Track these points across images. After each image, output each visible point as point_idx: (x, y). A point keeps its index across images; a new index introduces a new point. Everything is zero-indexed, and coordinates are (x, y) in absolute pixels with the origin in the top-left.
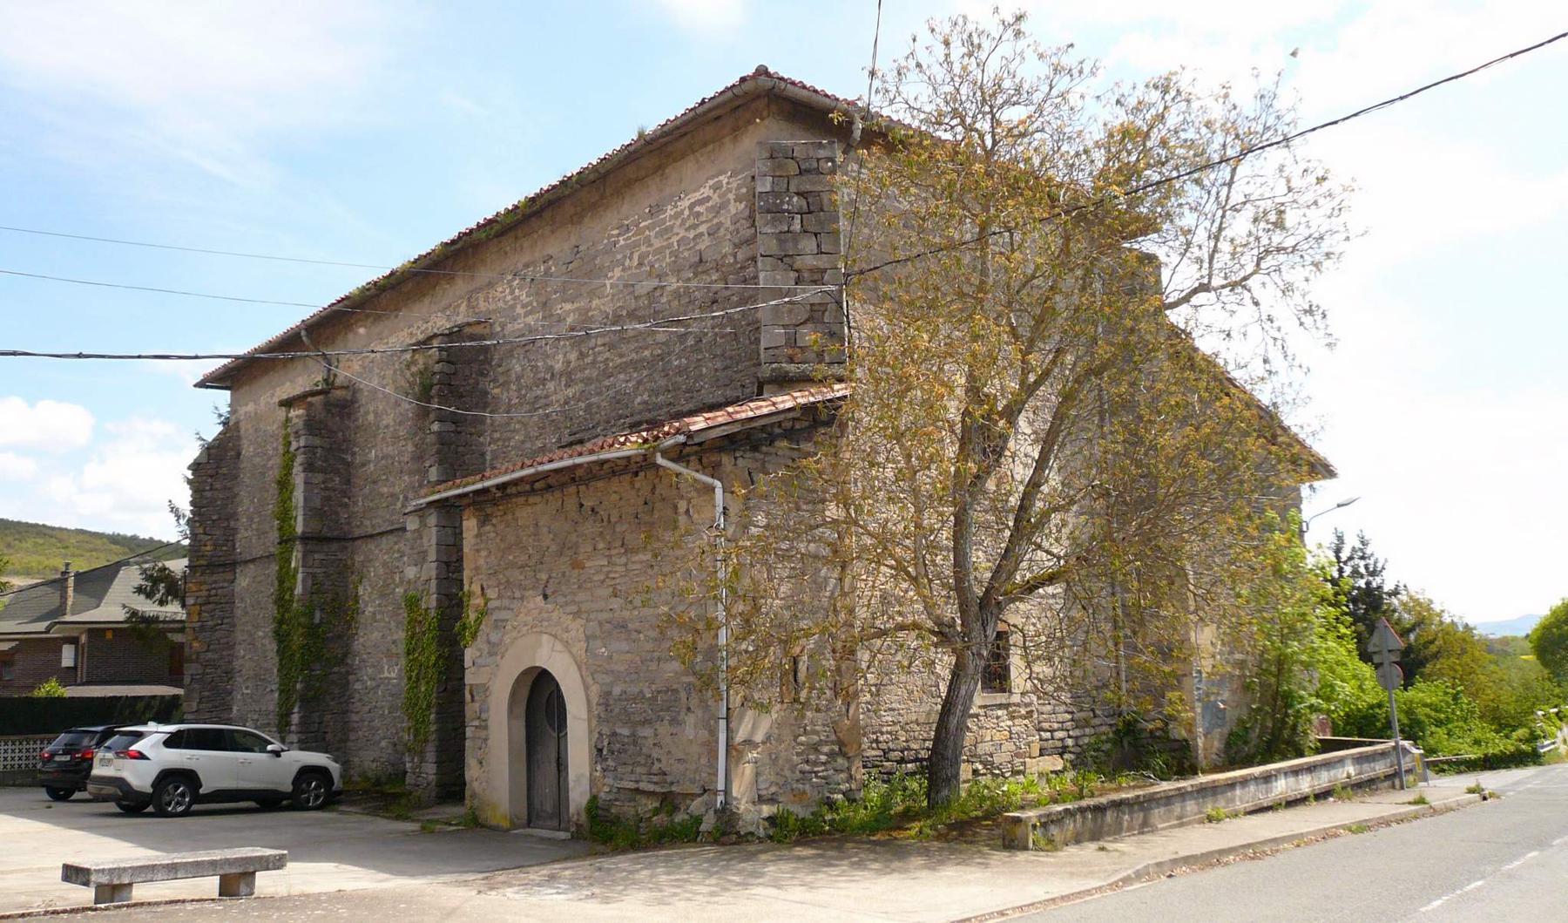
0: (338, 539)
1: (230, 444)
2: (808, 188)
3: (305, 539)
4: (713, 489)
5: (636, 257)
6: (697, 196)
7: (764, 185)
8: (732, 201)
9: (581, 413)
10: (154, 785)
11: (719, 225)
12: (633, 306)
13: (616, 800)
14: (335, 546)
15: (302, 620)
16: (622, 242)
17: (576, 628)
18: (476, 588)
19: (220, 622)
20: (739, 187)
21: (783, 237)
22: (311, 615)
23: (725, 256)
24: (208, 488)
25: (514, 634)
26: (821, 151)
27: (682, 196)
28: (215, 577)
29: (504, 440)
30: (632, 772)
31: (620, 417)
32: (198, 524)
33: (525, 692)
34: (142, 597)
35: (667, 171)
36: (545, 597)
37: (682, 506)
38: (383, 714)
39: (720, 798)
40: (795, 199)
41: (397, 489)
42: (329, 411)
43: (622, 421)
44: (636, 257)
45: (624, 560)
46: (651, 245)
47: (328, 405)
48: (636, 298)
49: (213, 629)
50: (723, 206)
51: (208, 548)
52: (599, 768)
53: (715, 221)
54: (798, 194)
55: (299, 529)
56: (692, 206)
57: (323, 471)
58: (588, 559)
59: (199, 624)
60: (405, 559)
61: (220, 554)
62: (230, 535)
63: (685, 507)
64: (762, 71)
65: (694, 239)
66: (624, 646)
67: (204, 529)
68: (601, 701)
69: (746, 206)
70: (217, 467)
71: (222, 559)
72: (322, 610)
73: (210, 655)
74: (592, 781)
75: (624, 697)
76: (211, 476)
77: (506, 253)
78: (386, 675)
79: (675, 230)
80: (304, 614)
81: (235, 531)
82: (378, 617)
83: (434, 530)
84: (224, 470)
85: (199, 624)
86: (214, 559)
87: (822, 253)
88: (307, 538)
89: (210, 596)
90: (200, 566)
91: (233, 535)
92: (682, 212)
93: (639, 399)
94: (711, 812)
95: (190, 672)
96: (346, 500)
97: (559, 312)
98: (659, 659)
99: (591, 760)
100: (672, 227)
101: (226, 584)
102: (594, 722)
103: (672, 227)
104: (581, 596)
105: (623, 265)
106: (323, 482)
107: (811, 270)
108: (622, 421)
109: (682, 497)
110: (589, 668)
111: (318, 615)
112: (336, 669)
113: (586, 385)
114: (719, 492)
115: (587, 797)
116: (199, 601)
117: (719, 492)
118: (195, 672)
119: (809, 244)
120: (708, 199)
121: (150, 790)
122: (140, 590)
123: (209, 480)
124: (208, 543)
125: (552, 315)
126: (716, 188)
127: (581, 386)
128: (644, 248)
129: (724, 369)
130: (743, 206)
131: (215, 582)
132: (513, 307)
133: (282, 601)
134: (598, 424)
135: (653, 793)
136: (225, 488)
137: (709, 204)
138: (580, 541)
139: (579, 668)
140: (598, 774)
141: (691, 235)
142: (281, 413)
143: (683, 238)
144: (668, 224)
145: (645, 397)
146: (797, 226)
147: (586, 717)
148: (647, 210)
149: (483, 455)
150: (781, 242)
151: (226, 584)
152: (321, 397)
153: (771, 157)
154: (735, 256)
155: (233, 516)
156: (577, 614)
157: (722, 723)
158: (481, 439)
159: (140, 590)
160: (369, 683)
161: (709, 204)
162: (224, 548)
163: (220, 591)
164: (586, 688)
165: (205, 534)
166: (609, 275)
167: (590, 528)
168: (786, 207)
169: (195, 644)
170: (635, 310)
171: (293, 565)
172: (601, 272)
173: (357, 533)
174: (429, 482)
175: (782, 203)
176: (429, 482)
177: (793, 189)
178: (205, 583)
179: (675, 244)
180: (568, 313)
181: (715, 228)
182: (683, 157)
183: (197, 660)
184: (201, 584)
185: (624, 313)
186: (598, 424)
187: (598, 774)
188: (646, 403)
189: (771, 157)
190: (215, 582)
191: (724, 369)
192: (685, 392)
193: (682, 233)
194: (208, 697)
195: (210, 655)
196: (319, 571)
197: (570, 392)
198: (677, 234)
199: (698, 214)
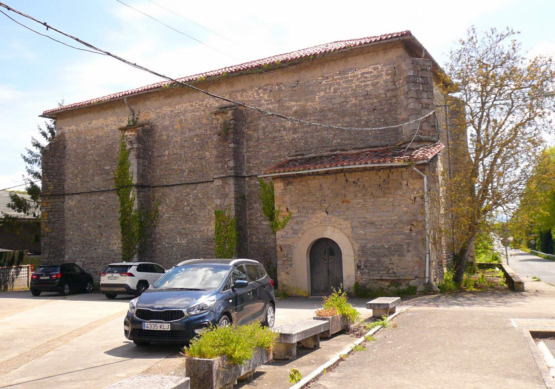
0: (148, 186)
1: (61, 143)
2: (424, 75)
3: (137, 186)
4: (422, 178)
5: (332, 89)
6: (365, 70)
7: (411, 73)
8: (384, 75)
9: (302, 144)
10: (137, 287)
11: (378, 83)
12: (332, 107)
13: (369, 283)
14: (147, 189)
15: (138, 219)
16: (324, 83)
17: (346, 224)
18: (283, 209)
19: (58, 219)
20: (387, 70)
21: (418, 91)
22: (140, 217)
23: (381, 94)
24: (51, 161)
25: (309, 226)
26: (427, 63)
27: (357, 69)
28: (54, 200)
29: (255, 152)
30: (378, 273)
31: (325, 147)
32: (46, 177)
33: (310, 248)
34: (10, 209)
35: (348, 59)
36: (327, 213)
37: (405, 183)
38: (177, 258)
39: (427, 280)
40: (420, 79)
41: (184, 168)
42: (143, 134)
43: (326, 149)
44: (332, 89)
45: (373, 200)
46: (341, 86)
47: (144, 131)
48: (333, 104)
49: (54, 222)
50: (379, 76)
51: (51, 188)
52: (359, 272)
53: (375, 81)
54: (421, 77)
55: (135, 181)
56: (362, 74)
57: (143, 158)
58: (352, 200)
59: (48, 220)
60: (191, 196)
61: (57, 190)
62: (61, 183)
63: (406, 183)
64: (408, 33)
65: (364, 86)
66: (374, 230)
67: (49, 179)
68: (360, 249)
69: (391, 77)
70: (55, 152)
71: (58, 192)
72: (144, 215)
73: (53, 234)
74: (356, 277)
75: (373, 247)
76: (52, 156)
77: (254, 79)
78: (179, 242)
79: (354, 82)
80: (138, 217)
81: (64, 181)
82: (172, 219)
83: (232, 186)
84: (58, 154)
85: (48, 220)
86: (54, 192)
87: (428, 98)
88: (139, 186)
89: (52, 208)
90: (47, 195)
91: (63, 182)
92: (357, 75)
93: (335, 141)
94: (422, 285)
95: (44, 241)
96: (150, 170)
97: (288, 105)
98: (393, 234)
99: (355, 270)
100: (352, 80)
101: (60, 203)
102: (356, 257)
103: (352, 80)
104: (348, 213)
105: (326, 91)
106: (143, 163)
107: (426, 104)
108: (326, 149)
109: (404, 180)
110: (354, 238)
111: (143, 217)
112: (148, 240)
113: (305, 134)
114: (425, 179)
115: (354, 283)
116: (47, 210)
117: (425, 179)
118: (46, 241)
119: (425, 95)
120: (371, 72)
121: (136, 289)
122: (9, 206)
123: (51, 158)
124: (51, 185)
125: (283, 106)
126: (375, 69)
127: (302, 134)
128: (336, 86)
129: (380, 134)
130: (389, 77)
131: (55, 202)
132: (260, 100)
133: (125, 212)
134: (312, 149)
135: (387, 280)
136: (58, 162)
137: (372, 74)
138: (347, 193)
139: (348, 238)
140: (358, 275)
141: (363, 84)
142: (120, 133)
143: (358, 85)
144: (350, 79)
145: (339, 141)
146: (421, 89)
147: (353, 255)
148: (338, 72)
149: (244, 157)
150: (417, 93)
151: (60, 203)
152: (141, 127)
153: (412, 63)
154: (386, 94)
155: (63, 174)
156: (345, 220)
157: (428, 255)
158: (243, 151)
159: (9, 206)
160: (167, 245)
161: (372, 74)
162: (59, 188)
163: (57, 206)
164: (352, 244)
165: (50, 181)
166: (317, 94)
167: (352, 189)
168: (418, 81)
169: (46, 229)
170: (332, 108)
171: (131, 196)
172: (313, 93)
173: (156, 184)
174: (228, 167)
175: (416, 80)
176: (228, 167)
177: (420, 75)
178: (50, 202)
179: (354, 87)
180: (294, 106)
181: (376, 83)
182: (357, 55)
183: (47, 236)
184: (48, 203)
185: (326, 109)
186: (312, 149)
187: (358, 275)
188: (338, 143)
189: (412, 63)
190: (55, 202)
191: (380, 134)
192: (360, 140)
193: (358, 83)
194: (52, 252)
195: (53, 234)
196: (142, 199)
197: (295, 136)
198: (355, 83)
199: (366, 77)
